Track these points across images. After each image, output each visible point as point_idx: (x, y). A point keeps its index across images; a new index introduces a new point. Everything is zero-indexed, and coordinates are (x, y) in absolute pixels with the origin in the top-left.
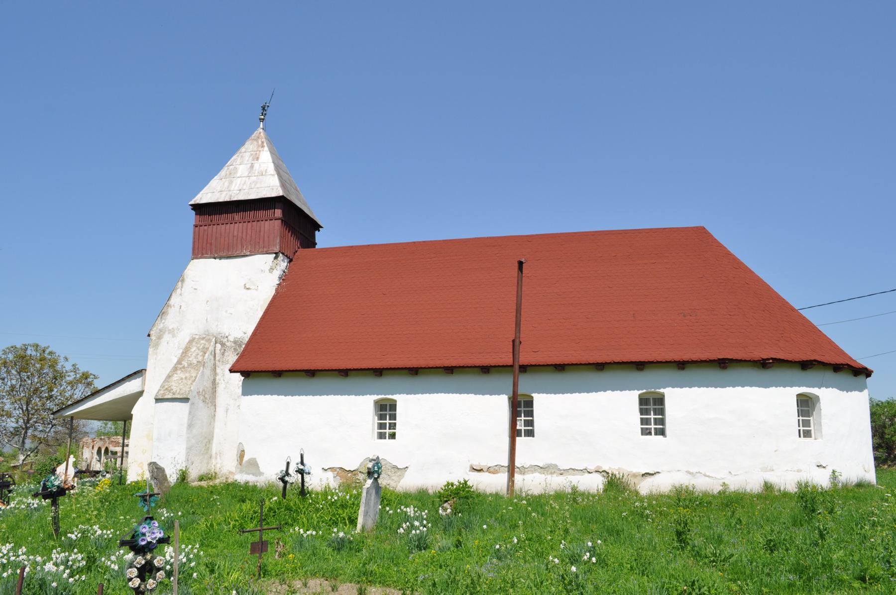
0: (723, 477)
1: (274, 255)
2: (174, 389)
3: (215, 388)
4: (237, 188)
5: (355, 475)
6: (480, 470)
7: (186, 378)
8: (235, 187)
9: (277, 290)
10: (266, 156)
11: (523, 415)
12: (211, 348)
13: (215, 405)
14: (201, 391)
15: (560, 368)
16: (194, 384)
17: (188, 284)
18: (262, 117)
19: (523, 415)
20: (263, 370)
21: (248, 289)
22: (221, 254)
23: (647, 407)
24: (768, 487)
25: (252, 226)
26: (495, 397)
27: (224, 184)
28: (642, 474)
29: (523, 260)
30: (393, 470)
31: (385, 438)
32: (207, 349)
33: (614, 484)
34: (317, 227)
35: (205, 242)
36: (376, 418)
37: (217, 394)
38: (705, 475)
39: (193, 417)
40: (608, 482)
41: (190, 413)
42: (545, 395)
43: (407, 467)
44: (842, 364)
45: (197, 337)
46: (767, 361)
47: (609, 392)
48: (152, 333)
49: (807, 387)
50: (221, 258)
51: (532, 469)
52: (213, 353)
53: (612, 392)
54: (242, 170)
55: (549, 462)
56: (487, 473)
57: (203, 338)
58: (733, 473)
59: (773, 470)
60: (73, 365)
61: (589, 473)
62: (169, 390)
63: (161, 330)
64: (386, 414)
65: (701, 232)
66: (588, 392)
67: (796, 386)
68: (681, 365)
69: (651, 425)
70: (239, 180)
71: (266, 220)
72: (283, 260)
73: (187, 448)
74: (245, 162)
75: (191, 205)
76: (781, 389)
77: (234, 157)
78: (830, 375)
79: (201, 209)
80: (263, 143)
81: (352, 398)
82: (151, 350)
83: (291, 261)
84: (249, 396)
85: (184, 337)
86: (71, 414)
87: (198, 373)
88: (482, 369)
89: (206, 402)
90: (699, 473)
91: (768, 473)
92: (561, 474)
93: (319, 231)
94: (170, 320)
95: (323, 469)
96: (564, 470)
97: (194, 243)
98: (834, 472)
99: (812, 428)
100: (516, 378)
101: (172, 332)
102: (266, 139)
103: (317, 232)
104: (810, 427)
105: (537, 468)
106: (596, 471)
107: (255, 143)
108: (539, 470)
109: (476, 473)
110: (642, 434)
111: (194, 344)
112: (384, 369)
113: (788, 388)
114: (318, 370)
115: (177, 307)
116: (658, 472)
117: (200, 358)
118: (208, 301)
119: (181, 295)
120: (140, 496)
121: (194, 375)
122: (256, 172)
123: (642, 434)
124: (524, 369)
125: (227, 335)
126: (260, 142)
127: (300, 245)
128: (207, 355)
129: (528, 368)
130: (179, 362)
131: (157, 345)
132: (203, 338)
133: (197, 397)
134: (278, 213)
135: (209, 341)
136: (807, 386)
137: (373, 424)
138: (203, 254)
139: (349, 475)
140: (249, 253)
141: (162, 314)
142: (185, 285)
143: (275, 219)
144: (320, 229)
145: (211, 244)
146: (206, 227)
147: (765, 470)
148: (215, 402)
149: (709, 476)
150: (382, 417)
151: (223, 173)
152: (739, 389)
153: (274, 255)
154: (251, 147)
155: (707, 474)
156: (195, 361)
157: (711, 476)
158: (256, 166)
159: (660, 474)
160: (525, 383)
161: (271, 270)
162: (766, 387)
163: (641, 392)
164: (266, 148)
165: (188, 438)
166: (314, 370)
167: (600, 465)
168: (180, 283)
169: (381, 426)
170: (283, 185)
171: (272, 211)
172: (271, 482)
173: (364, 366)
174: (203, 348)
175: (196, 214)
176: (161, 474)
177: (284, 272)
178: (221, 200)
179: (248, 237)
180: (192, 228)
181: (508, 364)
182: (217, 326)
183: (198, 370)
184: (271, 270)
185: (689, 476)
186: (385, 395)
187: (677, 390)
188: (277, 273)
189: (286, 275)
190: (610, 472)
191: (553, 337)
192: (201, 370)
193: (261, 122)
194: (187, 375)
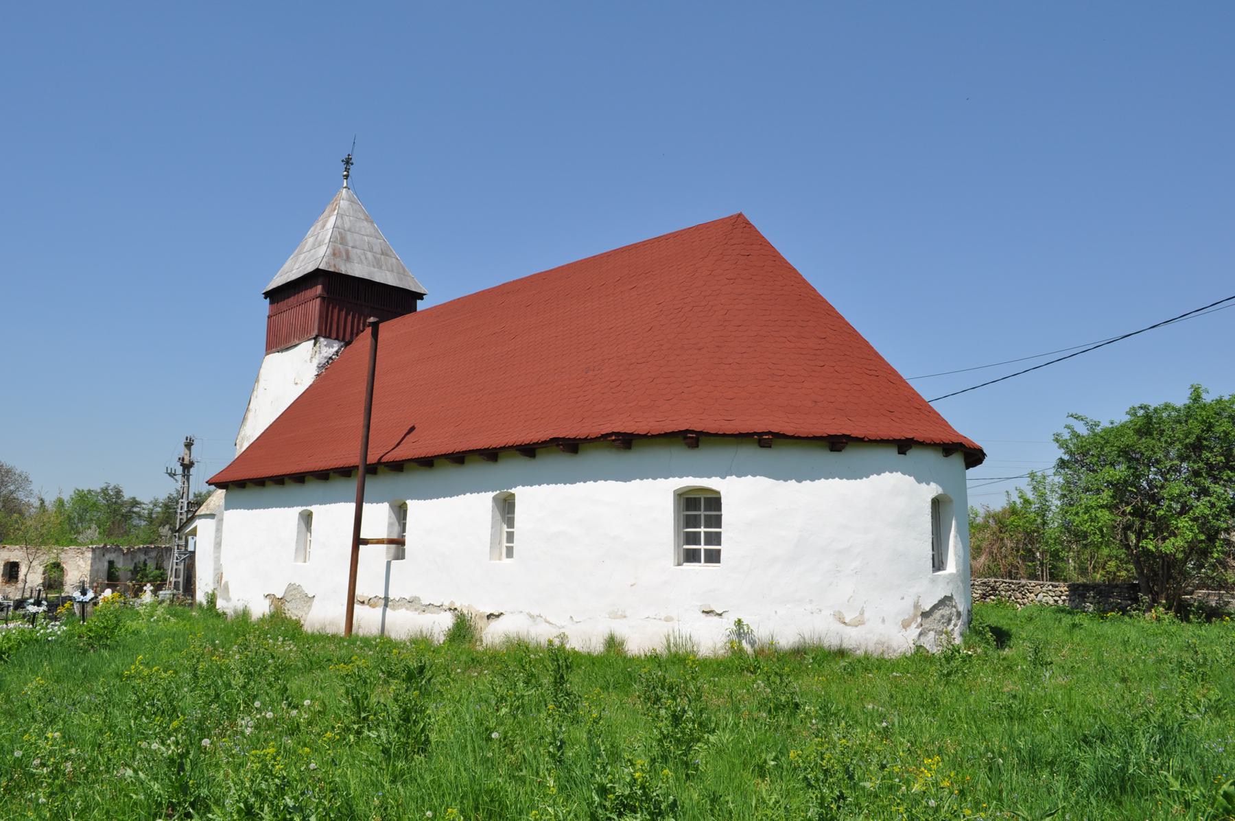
1: (313, 341)
18: (345, 173)
24: (613, 643)
26: (380, 505)
28: (486, 615)
43: (314, 596)
53: (826, 481)
56: (368, 606)
58: (575, 620)
59: (625, 617)
67: (674, 477)
69: (700, 544)
84: (792, 483)
91: (618, 620)
95: (703, 612)
98: (739, 623)
106: (450, 609)
110: (403, 558)
113: (661, 481)
116: (502, 614)
118: (272, 402)
123: (403, 558)
134: (319, 289)
136: (695, 476)
140: (297, 342)
144: (424, 297)
150: (691, 521)
152: (590, 484)
155: (548, 619)
157: (551, 622)
162: (625, 481)
163: (495, 493)
180: (266, 319)
181: (727, 433)
191: (683, 383)
193: (345, 181)
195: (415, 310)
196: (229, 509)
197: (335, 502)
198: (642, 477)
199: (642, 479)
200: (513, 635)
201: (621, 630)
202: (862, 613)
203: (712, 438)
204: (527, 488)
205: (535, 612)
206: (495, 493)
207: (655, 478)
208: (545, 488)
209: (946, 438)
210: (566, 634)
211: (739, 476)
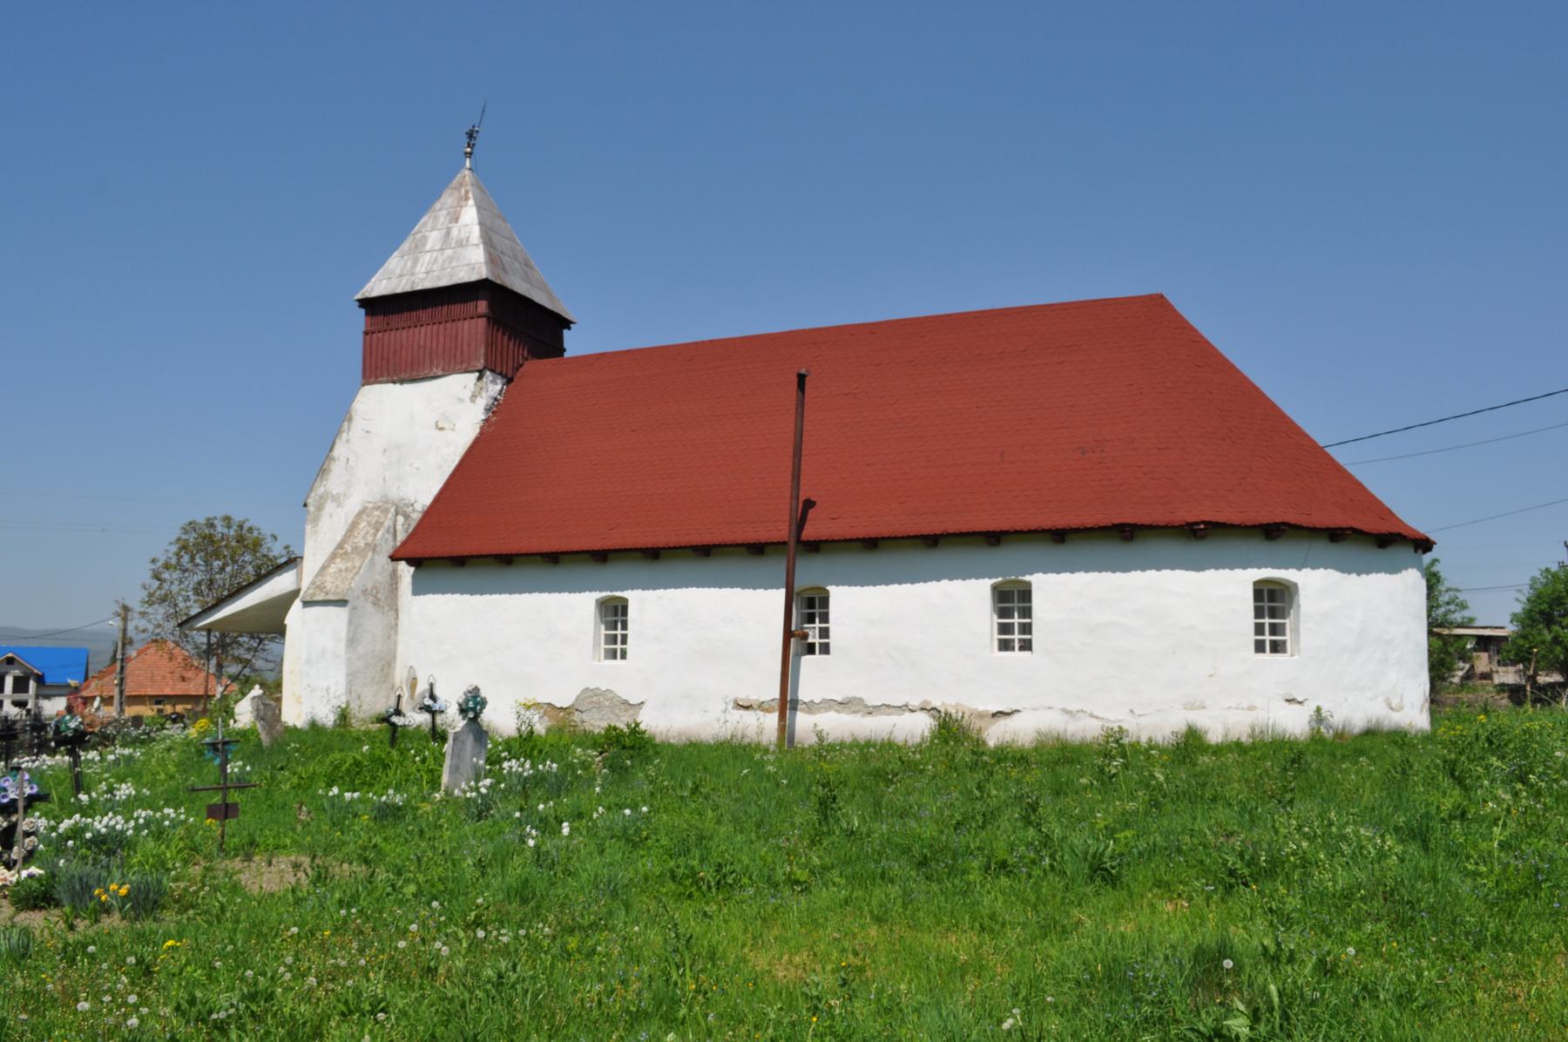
0: (1120, 718)
1: (477, 374)
2: (329, 586)
3: (397, 583)
4: (423, 270)
5: (569, 714)
6: (747, 708)
7: (347, 569)
8: (421, 269)
9: (482, 428)
10: (470, 214)
11: (1016, 614)
12: (388, 523)
13: (396, 610)
14: (369, 589)
15: (871, 544)
16: (357, 578)
17: (358, 424)
18: (469, 150)
19: (1016, 614)
20: (848, 537)
21: (441, 429)
22: (403, 376)
23: (811, 611)
25: (445, 329)
27: (405, 264)
29: (803, 371)
30: (622, 707)
31: (1013, 649)
32: (382, 523)
33: (949, 730)
34: (566, 324)
35: (380, 356)
36: (603, 627)
37: (400, 593)
38: (1092, 716)
39: (357, 628)
40: (939, 725)
41: (350, 622)
42: (673, 590)
43: (642, 703)
44: (1340, 529)
45: (370, 505)
46: (1196, 527)
47: (945, 582)
48: (310, 501)
49: (1273, 568)
50: (402, 382)
51: (827, 706)
52: (392, 530)
54: (434, 238)
55: (852, 694)
57: (378, 508)
58: (1137, 712)
59: (1204, 707)
60: (286, 547)
61: (912, 711)
62: (321, 588)
63: (321, 497)
64: (1013, 608)
65: (1157, 304)
66: (912, 583)
67: (1252, 567)
68: (1059, 536)
70: (429, 254)
71: (465, 319)
72: (494, 382)
73: (348, 675)
74: (439, 226)
75: (359, 300)
76: (1225, 573)
77: (424, 219)
78: (1322, 548)
79: (375, 307)
80: (467, 192)
81: (565, 597)
82: (308, 528)
83: (509, 381)
85: (352, 506)
86: (208, 624)
87: (363, 562)
88: (748, 548)
89: (378, 604)
90: (1082, 711)
92: (870, 713)
93: (569, 328)
94: (334, 482)
96: (874, 707)
97: (364, 359)
98: (1318, 710)
99: (1287, 637)
100: (791, 560)
101: (337, 499)
102: (473, 185)
103: (566, 332)
104: (1284, 635)
105: (832, 703)
106: (922, 709)
107: (456, 194)
108: (837, 708)
109: (742, 712)
111: (364, 517)
112: (609, 551)
113: (1238, 572)
114: (883, 539)
115: (343, 460)
116: (1018, 711)
117: (370, 539)
118: (385, 450)
119: (348, 441)
120: (208, 744)
121: (357, 564)
122: (453, 242)
124: (814, 547)
125: (412, 501)
126: (463, 192)
127: (528, 353)
128: (380, 534)
129: (561, 557)
130: (340, 546)
131: (316, 520)
132: (378, 508)
133: (362, 599)
134: (482, 306)
135: (386, 511)
137: (992, 625)
138: (377, 377)
139: (561, 714)
140: (440, 373)
141: (322, 471)
142: (353, 427)
143: (478, 317)
144: (572, 325)
145: (388, 360)
146: (380, 335)
147: (1189, 706)
148: (396, 605)
149: (1097, 717)
150: (1003, 613)
151: (406, 246)
153: (477, 374)
154: (449, 201)
155: (1095, 713)
156: (362, 544)
157: (1100, 716)
158: (455, 232)
159: (1020, 714)
160: (809, 573)
161: (473, 397)
163: (994, 581)
164: (471, 202)
165: (349, 659)
166: (877, 538)
167: (928, 698)
168: (346, 423)
169: (1005, 629)
170: (493, 259)
171: (473, 304)
172: (1347, 729)
173: (576, 547)
174: (377, 522)
175: (367, 314)
176: (269, 713)
177: (496, 399)
178: (399, 291)
179: (440, 348)
180: (361, 336)
182: (398, 488)
183: (365, 557)
184: (473, 397)
185: (1066, 717)
186: (612, 591)
187: (1052, 577)
188: (482, 402)
189: (499, 405)
190: (943, 710)
192: (369, 557)
193: (468, 160)
194: (349, 565)
196: (424, 593)
201: (1201, 720)
202: (1402, 699)
204: (1052, 577)
205: (1073, 707)
206: (994, 581)
207: (1232, 568)
209: (1384, 528)
211: (1313, 568)
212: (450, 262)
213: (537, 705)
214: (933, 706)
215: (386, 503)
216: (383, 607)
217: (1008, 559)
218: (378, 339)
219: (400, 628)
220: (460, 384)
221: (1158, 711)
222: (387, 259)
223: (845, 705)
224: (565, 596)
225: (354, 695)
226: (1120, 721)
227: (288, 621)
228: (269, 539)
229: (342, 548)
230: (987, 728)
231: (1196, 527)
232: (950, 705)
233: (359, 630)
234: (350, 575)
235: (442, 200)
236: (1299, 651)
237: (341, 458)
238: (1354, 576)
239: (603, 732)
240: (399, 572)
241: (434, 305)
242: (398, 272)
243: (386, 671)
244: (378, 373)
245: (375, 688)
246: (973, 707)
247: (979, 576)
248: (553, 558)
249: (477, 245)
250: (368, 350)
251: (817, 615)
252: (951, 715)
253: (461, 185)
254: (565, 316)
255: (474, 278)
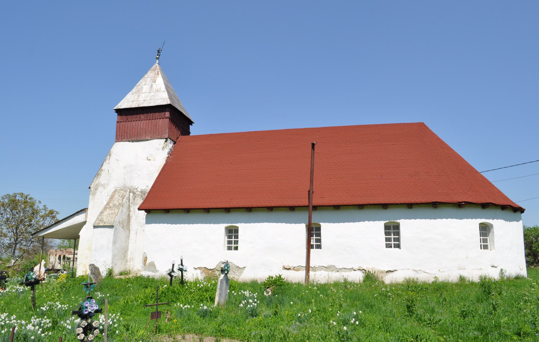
0: (435, 273)
1: (165, 140)
3: (130, 219)
4: (142, 99)
5: (213, 272)
7: (112, 213)
8: (141, 99)
9: (166, 161)
11: (314, 236)
12: (127, 196)
13: (129, 230)
15: (337, 207)
16: (117, 217)
18: (158, 57)
19: (314, 236)
21: (149, 160)
22: (133, 139)
25: (152, 122)
29: (315, 143)
32: (125, 196)
33: (369, 277)
34: (191, 123)
35: (123, 131)
38: (424, 272)
39: (116, 237)
40: (366, 276)
41: (114, 234)
43: (245, 267)
44: (507, 205)
45: (119, 189)
46: (461, 204)
47: (366, 222)
48: (91, 186)
50: (133, 141)
51: (320, 268)
52: (128, 198)
54: (146, 88)
56: (293, 271)
58: (441, 271)
59: (465, 269)
60: (44, 206)
61: (355, 270)
62: (101, 220)
63: (97, 185)
64: (232, 235)
65: (422, 126)
68: (410, 206)
70: (144, 95)
73: (112, 256)
74: (148, 84)
75: (115, 110)
76: (470, 220)
77: (141, 81)
78: (499, 212)
79: (120, 112)
80: (158, 72)
82: (91, 197)
83: (175, 143)
85: (110, 189)
86: (43, 235)
87: (119, 210)
90: (421, 270)
91: (462, 270)
92: (338, 271)
93: (192, 125)
94: (102, 179)
96: (339, 269)
97: (117, 132)
98: (502, 270)
99: (488, 244)
101: (103, 186)
103: (190, 126)
105: (323, 267)
106: (359, 270)
107: (154, 72)
108: (324, 269)
109: (286, 271)
110: (386, 247)
111: (117, 193)
113: (474, 220)
116: (396, 270)
117: (120, 202)
118: (125, 167)
119: (109, 163)
120: (84, 285)
121: (117, 212)
122: (154, 90)
123: (386, 247)
124: (315, 208)
125: (136, 187)
126: (156, 72)
128: (124, 199)
130: (108, 204)
131: (94, 194)
134: (167, 114)
135: (126, 191)
137: (225, 241)
139: (210, 272)
140: (149, 139)
141: (97, 175)
143: (166, 118)
144: (193, 124)
145: (127, 133)
147: (460, 268)
148: (129, 228)
149: (426, 273)
150: (230, 237)
151: (134, 90)
152: (444, 220)
153: (165, 140)
154: (151, 74)
155: (426, 271)
156: (117, 204)
158: (154, 86)
160: (316, 217)
161: (163, 148)
164: (160, 75)
165: (113, 249)
168: (108, 156)
169: (229, 242)
170: (170, 98)
171: (163, 113)
172: (163, 276)
176: (97, 271)
177: (171, 150)
180: (116, 123)
182: (131, 182)
183: (119, 209)
184: (163, 148)
185: (415, 273)
188: (167, 150)
190: (367, 270)
192: (121, 209)
193: (157, 60)
194: (113, 212)
195: (189, 135)
197: (344, 222)
198: (421, 218)
199: (467, 219)
200: (407, 278)
203: (348, 206)
208: (418, 220)
210: (437, 276)
212: (154, 97)
213: (199, 268)
214: (363, 269)
215: (125, 188)
216: (125, 229)
217: (391, 215)
218: (123, 125)
219: (130, 237)
220: (159, 143)
221: (449, 270)
222: (127, 95)
223: (327, 268)
224: (212, 225)
225: (114, 264)
226: (435, 274)
227: (81, 234)
228: (37, 202)
229: (109, 205)
230: (384, 277)
231: (461, 204)
232: (370, 268)
233: (117, 238)
234: (114, 216)
235: (148, 74)
236: (494, 248)
237: (106, 170)
238: (508, 222)
239: (477, 282)
240: (131, 215)
241: (147, 113)
242: (132, 100)
243: (125, 254)
244: (123, 138)
245: (121, 261)
246: (379, 269)
247: (379, 220)
248: (207, 210)
249: (164, 91)
250: (118, 129)
251: (314, 234)
252: (370, 272)
253: (155, 69)
254: (192, 120)
255: (165, 103)
